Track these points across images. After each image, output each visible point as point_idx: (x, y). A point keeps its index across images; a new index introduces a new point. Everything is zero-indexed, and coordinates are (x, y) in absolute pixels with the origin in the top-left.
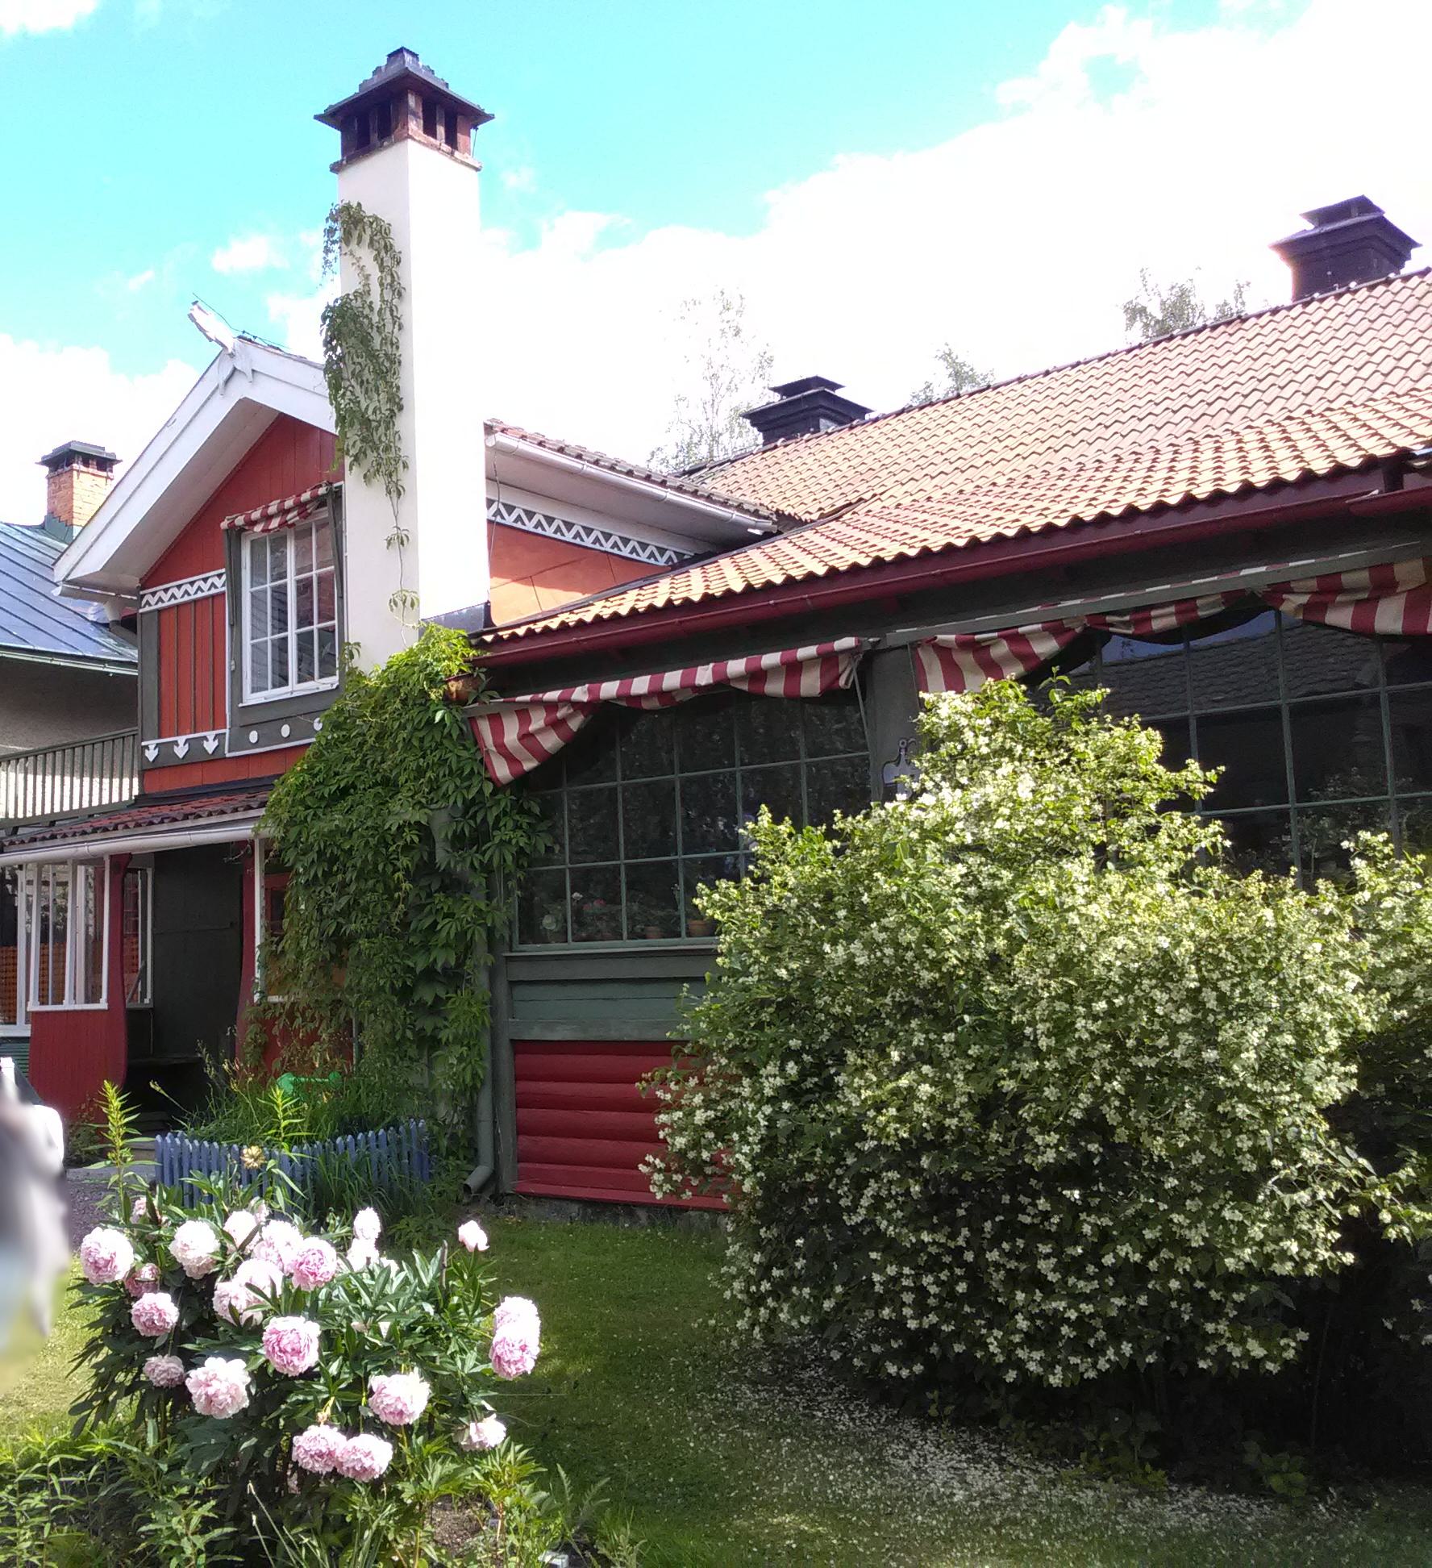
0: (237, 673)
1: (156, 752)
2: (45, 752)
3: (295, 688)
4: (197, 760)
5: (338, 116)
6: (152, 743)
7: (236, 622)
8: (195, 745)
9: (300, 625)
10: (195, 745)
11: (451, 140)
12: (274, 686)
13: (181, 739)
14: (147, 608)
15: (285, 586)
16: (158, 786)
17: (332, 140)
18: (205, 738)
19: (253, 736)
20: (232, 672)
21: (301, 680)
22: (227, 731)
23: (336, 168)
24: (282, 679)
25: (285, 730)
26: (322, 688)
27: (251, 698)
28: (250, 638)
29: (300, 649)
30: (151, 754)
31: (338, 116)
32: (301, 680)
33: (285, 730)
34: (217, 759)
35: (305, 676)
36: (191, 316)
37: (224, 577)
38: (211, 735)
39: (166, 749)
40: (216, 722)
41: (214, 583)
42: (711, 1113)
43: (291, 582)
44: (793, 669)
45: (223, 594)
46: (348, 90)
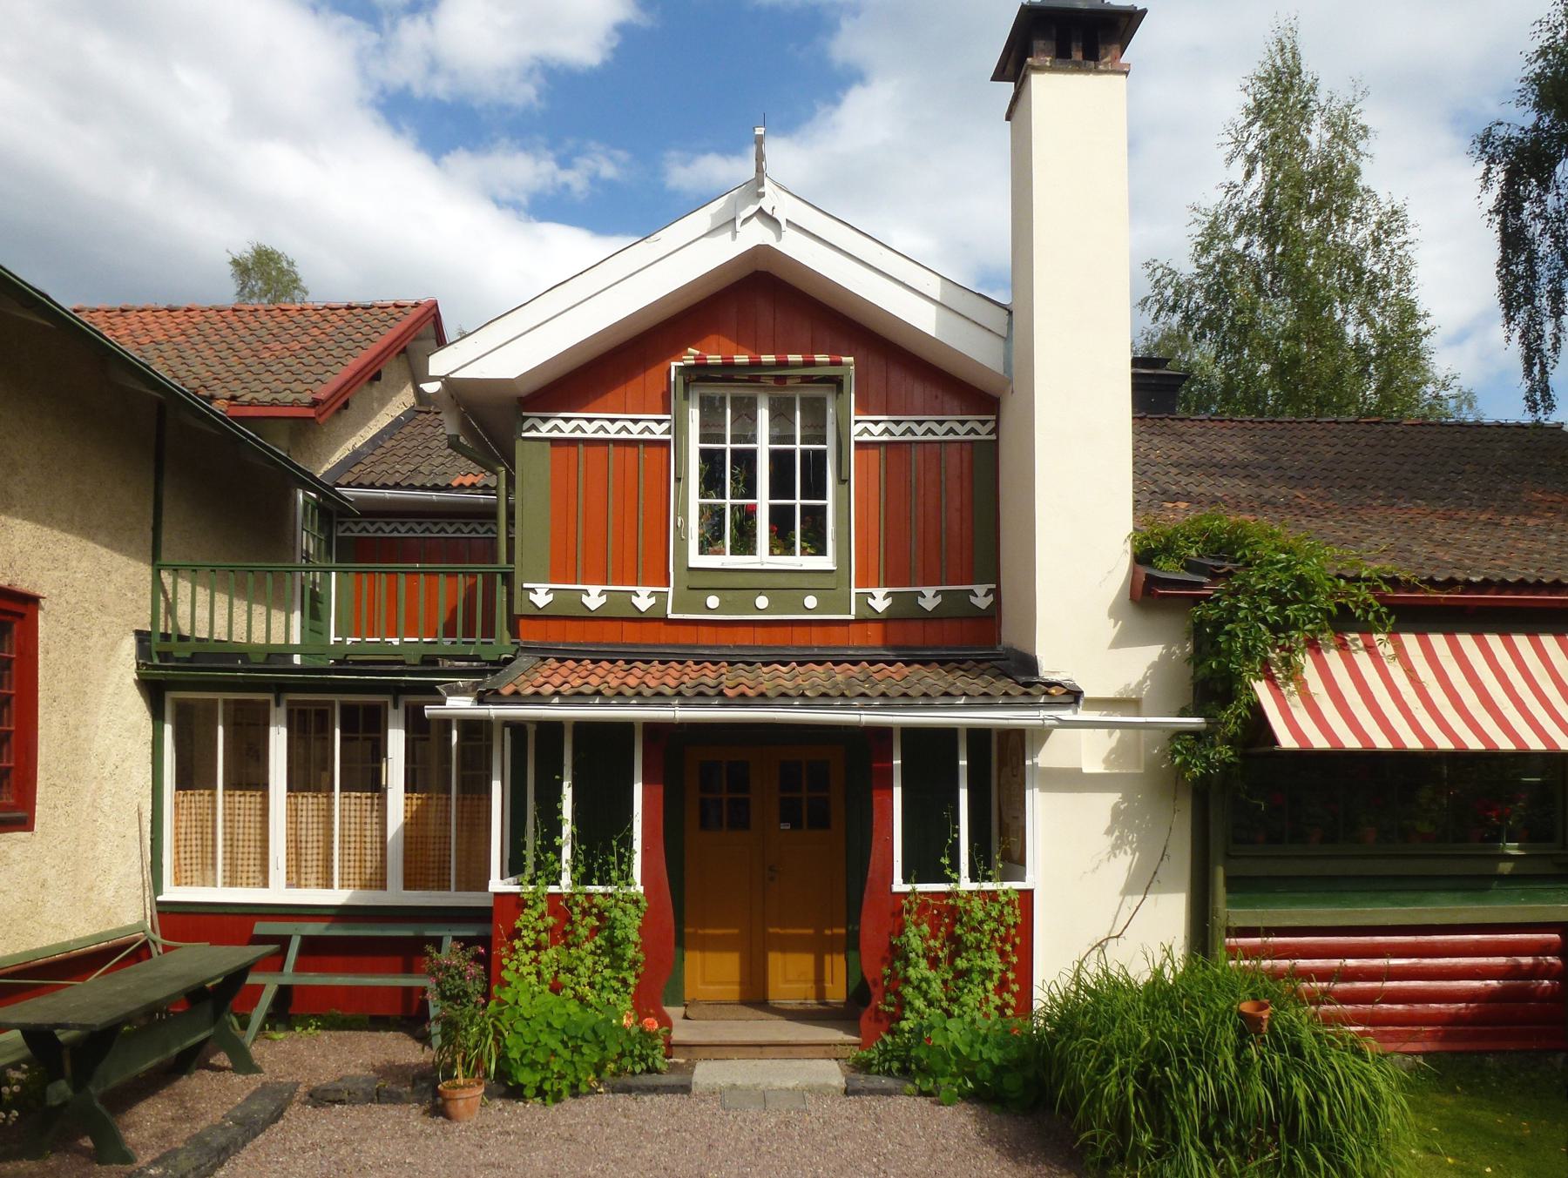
3: (763, 558)
4: (619, 616)
6: (542, 588)
9: (753, 454)
13: (594, 590)
14: (533, 434)
22: (670, 590)
24: (744, 542)
27: (696, 560)
34: (654, 619)
37: (665, 426)
38: (644, 591)
45: (666, 443)
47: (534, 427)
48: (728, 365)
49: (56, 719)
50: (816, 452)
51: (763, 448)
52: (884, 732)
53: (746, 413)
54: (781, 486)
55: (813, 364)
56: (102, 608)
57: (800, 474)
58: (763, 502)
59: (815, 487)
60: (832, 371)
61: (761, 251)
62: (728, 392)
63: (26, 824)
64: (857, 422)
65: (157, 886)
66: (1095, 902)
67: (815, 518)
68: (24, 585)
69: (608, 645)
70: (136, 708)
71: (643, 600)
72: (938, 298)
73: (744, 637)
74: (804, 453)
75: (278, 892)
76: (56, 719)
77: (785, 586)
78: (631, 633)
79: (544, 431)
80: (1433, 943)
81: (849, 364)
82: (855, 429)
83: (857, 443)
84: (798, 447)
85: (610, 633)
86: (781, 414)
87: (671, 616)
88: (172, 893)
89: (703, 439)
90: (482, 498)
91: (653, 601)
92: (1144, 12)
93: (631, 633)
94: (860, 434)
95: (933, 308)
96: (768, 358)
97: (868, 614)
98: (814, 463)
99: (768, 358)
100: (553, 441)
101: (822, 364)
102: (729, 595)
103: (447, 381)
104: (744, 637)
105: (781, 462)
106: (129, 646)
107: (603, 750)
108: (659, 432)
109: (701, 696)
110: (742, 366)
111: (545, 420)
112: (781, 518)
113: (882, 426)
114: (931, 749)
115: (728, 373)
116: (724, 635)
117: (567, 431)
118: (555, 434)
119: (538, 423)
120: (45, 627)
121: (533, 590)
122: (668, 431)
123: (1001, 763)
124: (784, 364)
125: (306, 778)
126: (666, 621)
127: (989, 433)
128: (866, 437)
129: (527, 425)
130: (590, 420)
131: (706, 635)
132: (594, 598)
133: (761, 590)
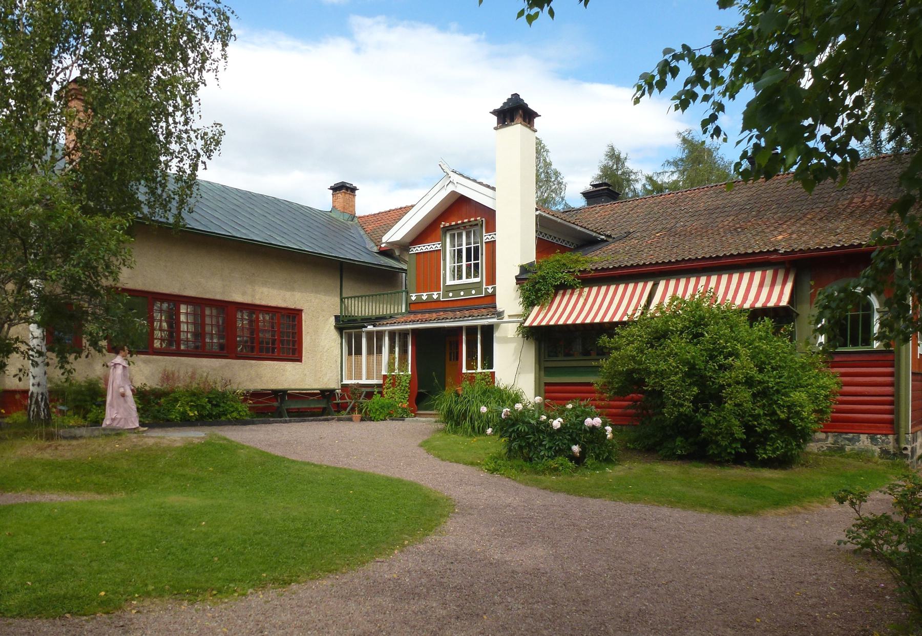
0: (445, 275)
2: (358, 297)
3: (464, 280)
4: (430, 301)
5: (496, 113)
6: (414, 295)
7: (445, 260)
8: (430, 296)
10: (430, 296)
11: (613, 149)
16: (413, 308)
17: (494, 119)
19: (451, 295)
21: (467, 278)
23: (496, 129)
24: (460, 278)
25: (473, 292)
27: (449, 282)
28: (449, 263)
30: (413, 298)
31: (496, 113)
32: (467, 278)
33: (473, 292)
34: (438, 301)
35: (468, 276)
36: (493, 189)
39: (419, 297)
41: (436, 246)
44: (161, 329)
46: (498, 105)
49: (308, 337)
52: (461, 328)
53: (460, 235)
54: (468, 259)
56: (323, 310)
58: (464, 263)
59: (476, 258)
63: (300, 360)
65: (342, 381)
66: (513, 369)
68: (298, 307)
70: (335, 335)
75: (364, 381)
76: (308, 337)
78: (433, 305)
80: (849, 418)
82: (484, 238)
85: (429, 306)
86: (468, 237)
88: (345, 382)
90: (594, 234)
93: (433, 305)
96: (460, 222)
104: (459, 304)
105: (468, 250)
106: (333, 319)
107: (404, 334)
109: (422, 322)
114: (472, 330)
115: (457, 227)
116: (477, 301)
120: (304, 316)
123: (488, 332)
124: (463, 223)
125: (370, 352)
131: (450, 305)
133: (462, 290)
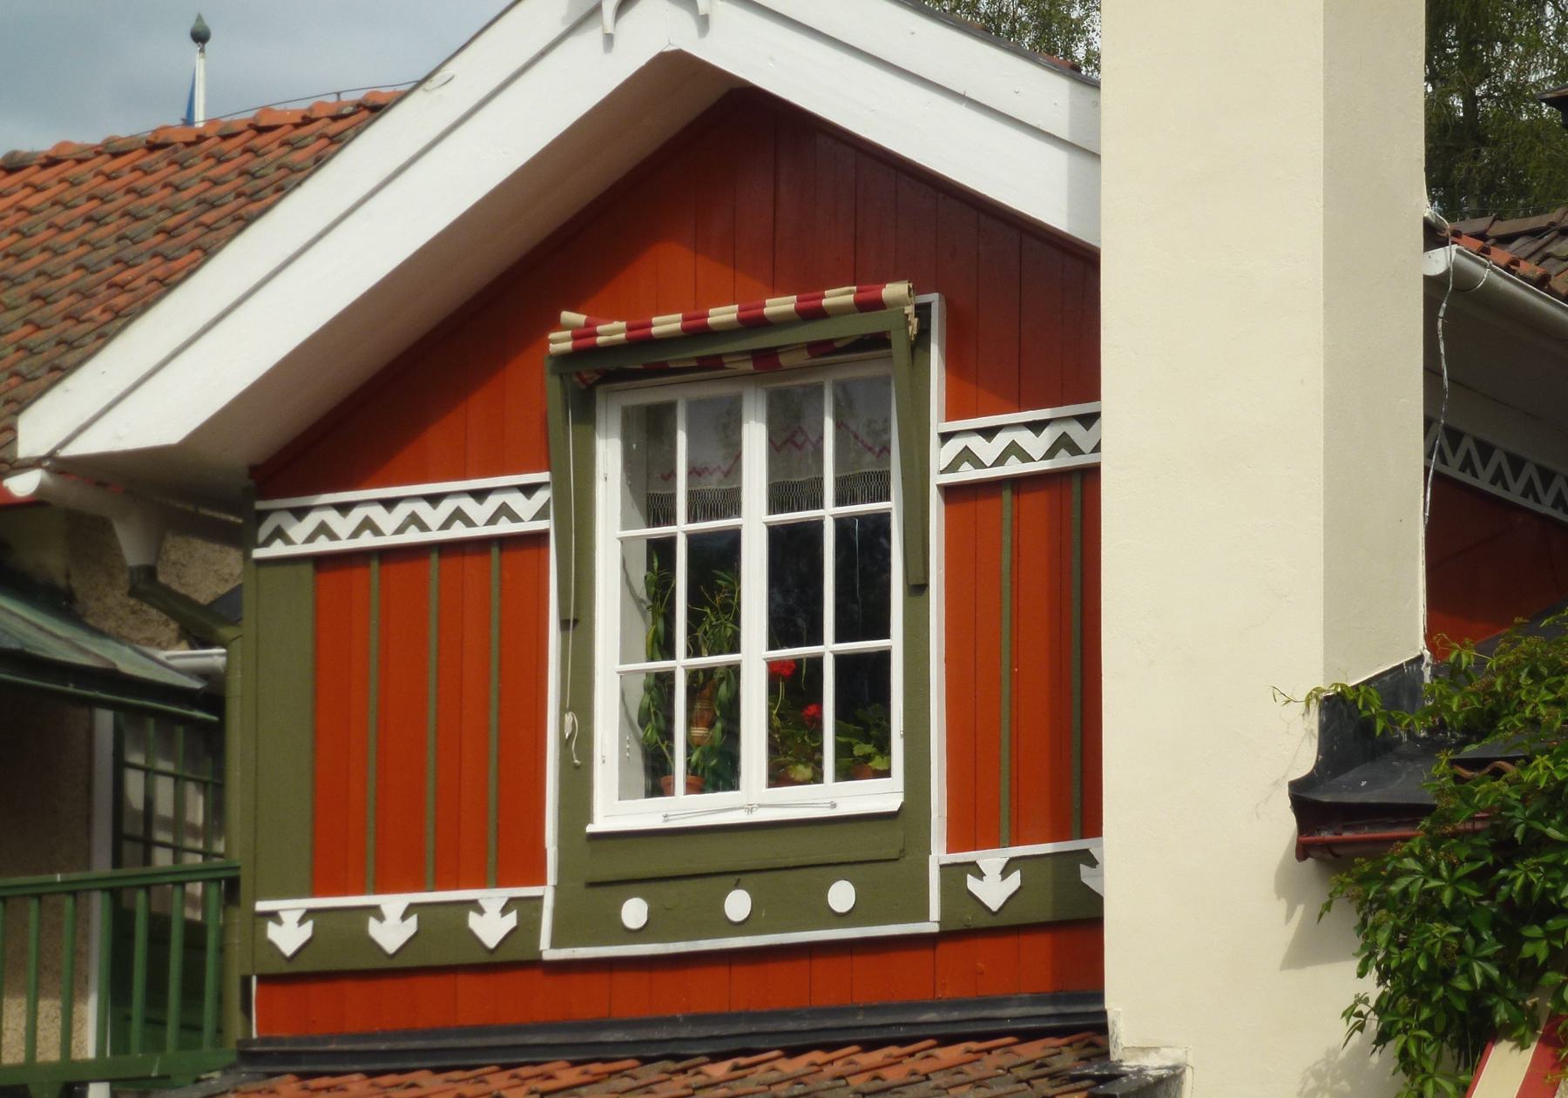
1: (307, 930)
3: (755, 798)
4: (443, 960)
7: (578, 622)
9: (732, 541)
12: (694, 787)
13: (393, 904)
14: (278, 549)
15: (734, 536)
18: (375, 911)
20: (564, 743)
21: (778, 777)
22: (547, 893)
24: (717, 771)
26: (846, 808)
27: (617, 808)
29: (732, 611)
32: (778, 777)
33: (842, 896)
34: (513, 961)
35: (792, 758)
37: (542, 496)
38: (493, 898)
40: (521, 863)
41: (513, 505)
42: (719, 725)
43: (754, 523)
45: (540, 538)
47: (279, 533)
48: (641, 342)
50: (864, 518)
51: (754, 523)
54: (792, 622)
55: (820, 314)
57: (828, 579)
58: (754, 655)
59: (864, 614)
60: (868, 324)
61: (673, 70)
62: (681, 397)
64: (945, 437)
67: (864, 682)
69: (425, 1034)
71: (491, 925)
72: (1064, 134)
73: (707, 992)
74: (842, 524)
77: (783, 860)
78: (472, 1002)
79: (300, 538)
81: (898, 303)
82: (940, 456)
83: (949, 491)
84: (829, 512)
86: (790, 442)
87: (549, 953)
89: (776, 505)
91: (511, 920)
92: (199, 18)
94: (953, 467)
95: (1060, 156)
96: (723, 314)
97: (971, 919)
98: (864, 545)
99: (780, 305)
100: (321, 562)
101: (840, 311)
102: (671, 891)
103: (56, 464)
104: (707, 992)
105: (792, 551)
108: (528, 514)
110: (668, 341)
111: (300, 513)
112: (793, 689)
113: (1049, 436)
117: (345, 534)
118: (323, 545)
119: (285, 520)
121: (273, 916)
122: (542, 514)
124: (754, 323)
126: (538, 964)
127: (536, 517)
128: (967, 474)
129: (265, 530)
130: (389, 504)
132: (392, 925)
133: (737, 876)
